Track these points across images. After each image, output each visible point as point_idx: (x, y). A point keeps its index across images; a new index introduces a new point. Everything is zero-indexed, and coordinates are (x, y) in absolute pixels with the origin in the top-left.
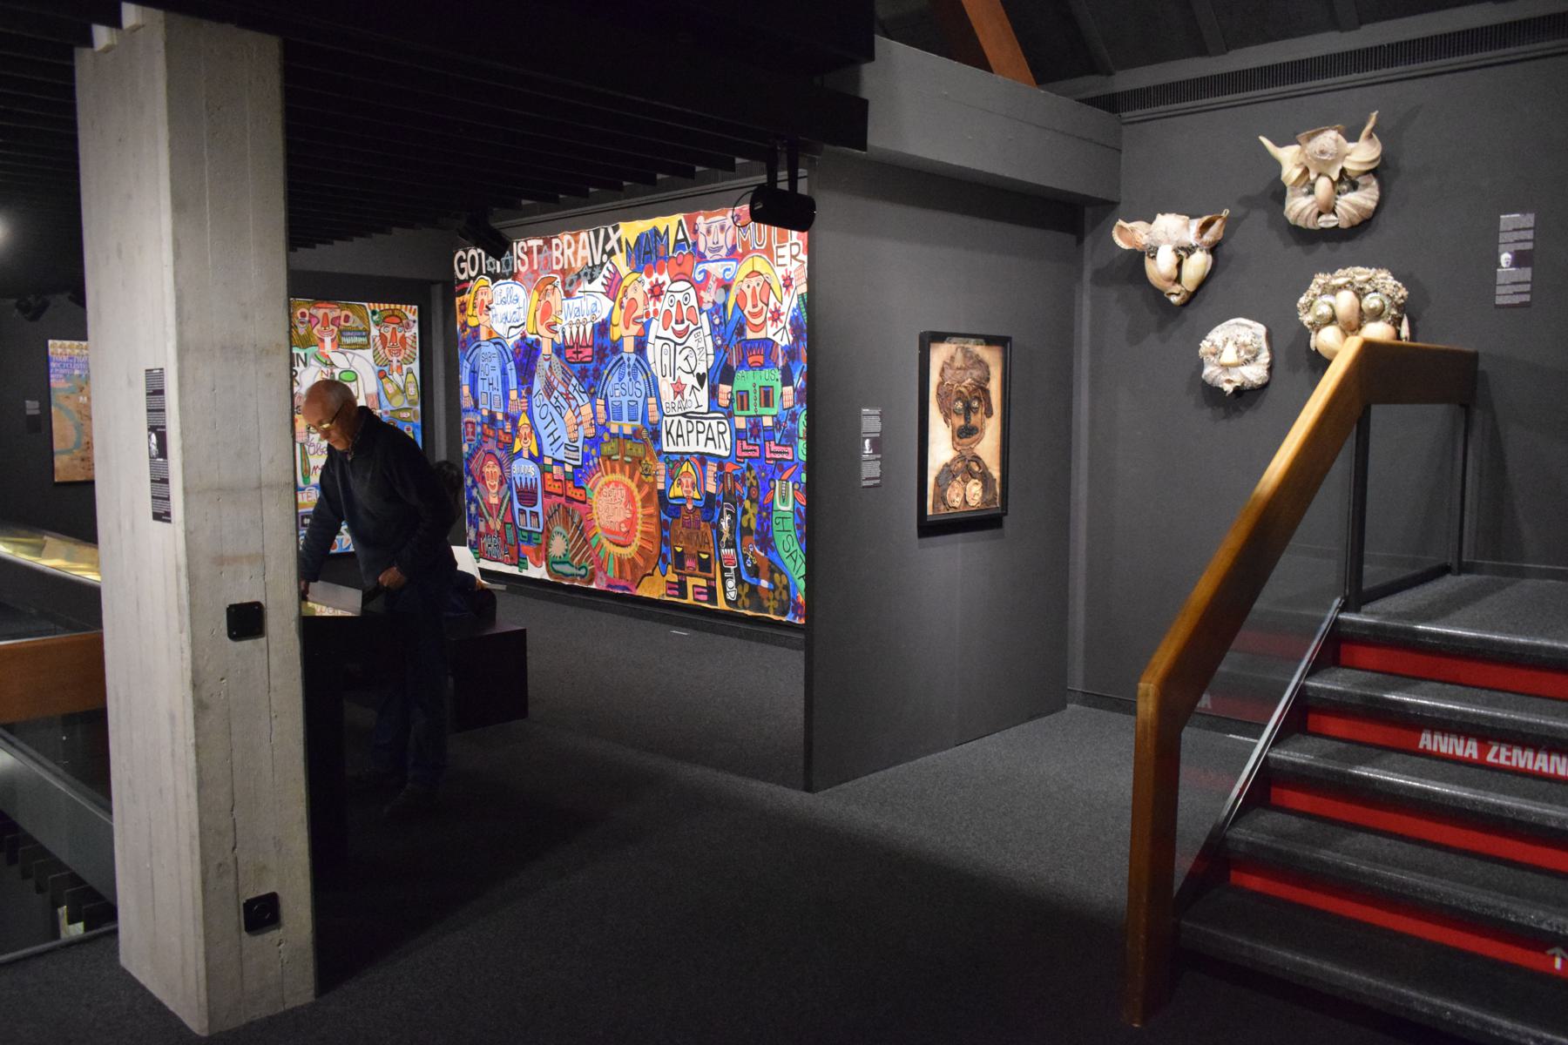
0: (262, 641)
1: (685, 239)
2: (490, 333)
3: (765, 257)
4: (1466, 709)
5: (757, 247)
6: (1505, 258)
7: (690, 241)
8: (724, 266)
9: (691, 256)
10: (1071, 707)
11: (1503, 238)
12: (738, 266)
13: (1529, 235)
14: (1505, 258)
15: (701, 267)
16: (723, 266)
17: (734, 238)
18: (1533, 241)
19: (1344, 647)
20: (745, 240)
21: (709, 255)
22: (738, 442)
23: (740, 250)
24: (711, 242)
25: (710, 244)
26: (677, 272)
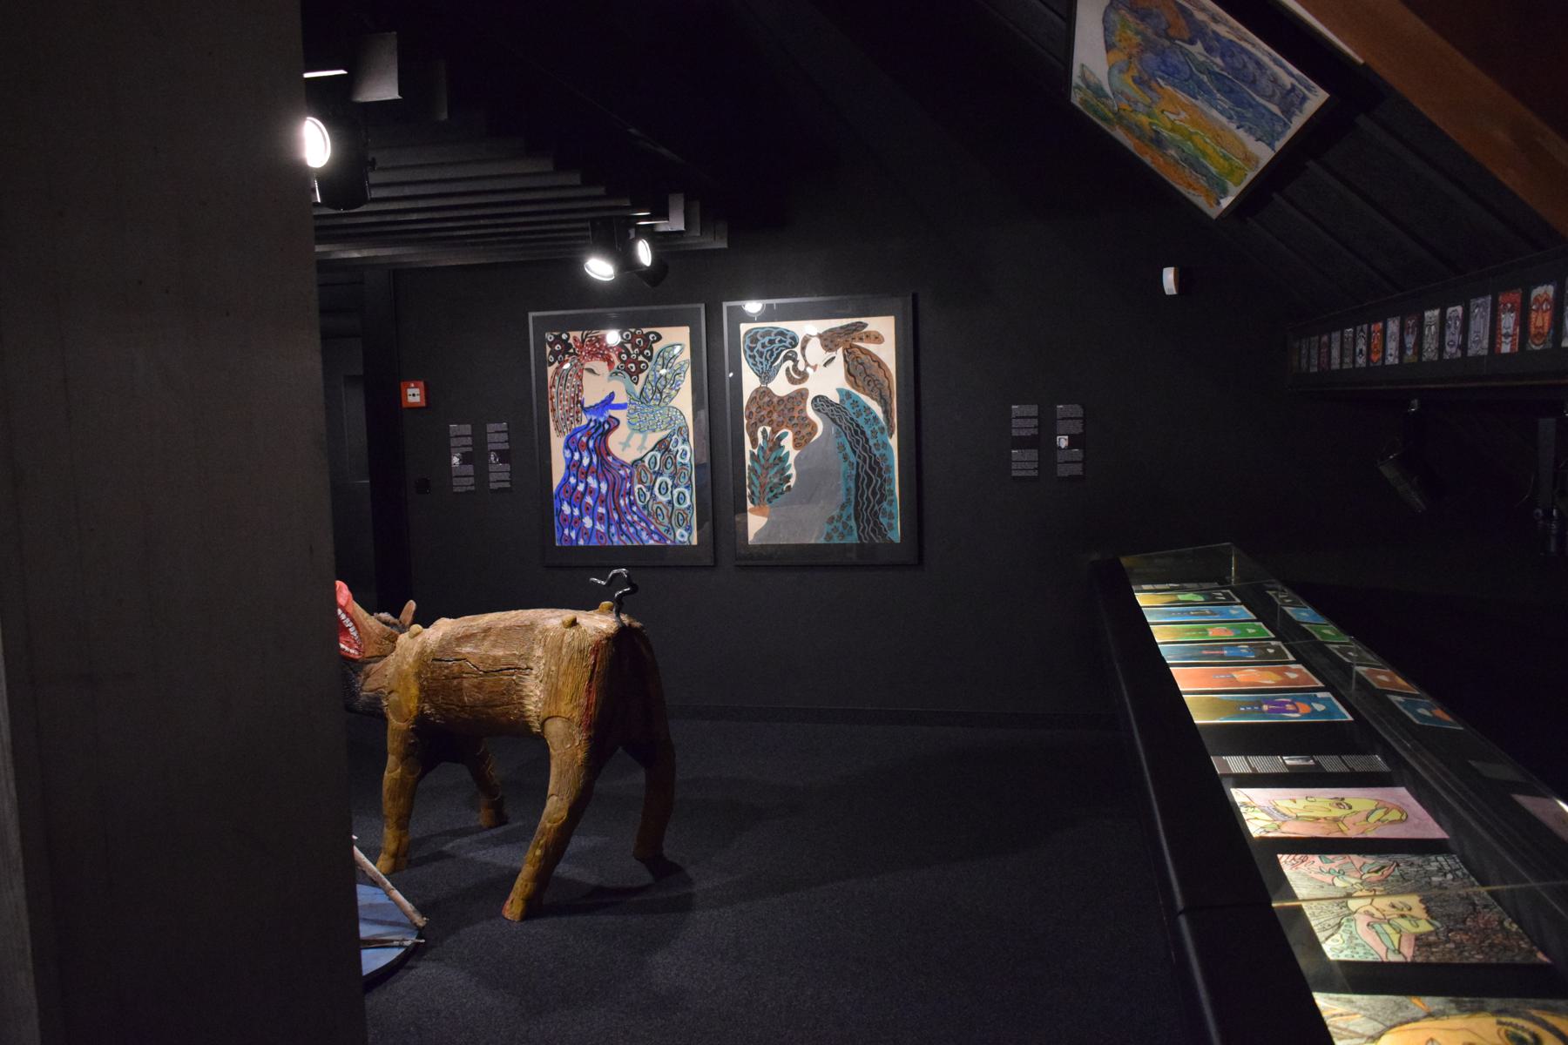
6: (455, 460)
11: (454, 442)
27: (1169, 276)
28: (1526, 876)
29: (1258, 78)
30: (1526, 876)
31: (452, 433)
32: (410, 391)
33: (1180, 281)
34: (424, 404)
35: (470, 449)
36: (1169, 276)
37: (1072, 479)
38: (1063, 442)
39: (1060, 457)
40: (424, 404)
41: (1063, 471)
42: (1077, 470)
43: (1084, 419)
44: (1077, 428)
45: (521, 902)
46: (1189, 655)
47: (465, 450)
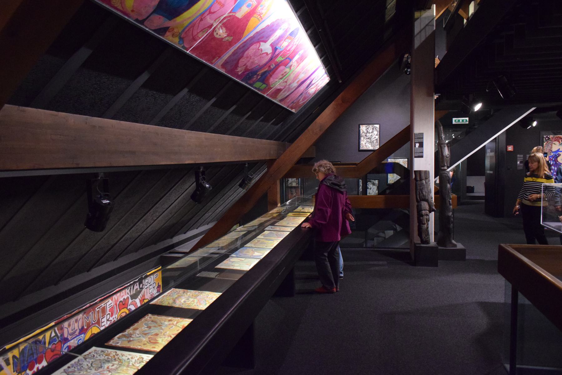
0: (373, 241)
1: (56, 335)
2: (157, 335)
3: (97, 325)
4: (137, 24)
5: (93, 322)
6: (518, 163)
7: (59, 335)
8: (77, 339)
9: (60, 343)
10: (417, 203)
11: (518, 159)
12: (85, 335)
13: (522, 158)
14: (518, 163)
15: (66, 345)
16: (77, 339)
17: (83, 322)
18: (523, 157)
19: (361, 148)
20: (88, 322)
21: (70, 337)
22: (298, 286)
23: (85, 327)
24: (71, 330)
25: (70, 331)
26: (52, 356)
32: (511, 148)
40: (513, 150)
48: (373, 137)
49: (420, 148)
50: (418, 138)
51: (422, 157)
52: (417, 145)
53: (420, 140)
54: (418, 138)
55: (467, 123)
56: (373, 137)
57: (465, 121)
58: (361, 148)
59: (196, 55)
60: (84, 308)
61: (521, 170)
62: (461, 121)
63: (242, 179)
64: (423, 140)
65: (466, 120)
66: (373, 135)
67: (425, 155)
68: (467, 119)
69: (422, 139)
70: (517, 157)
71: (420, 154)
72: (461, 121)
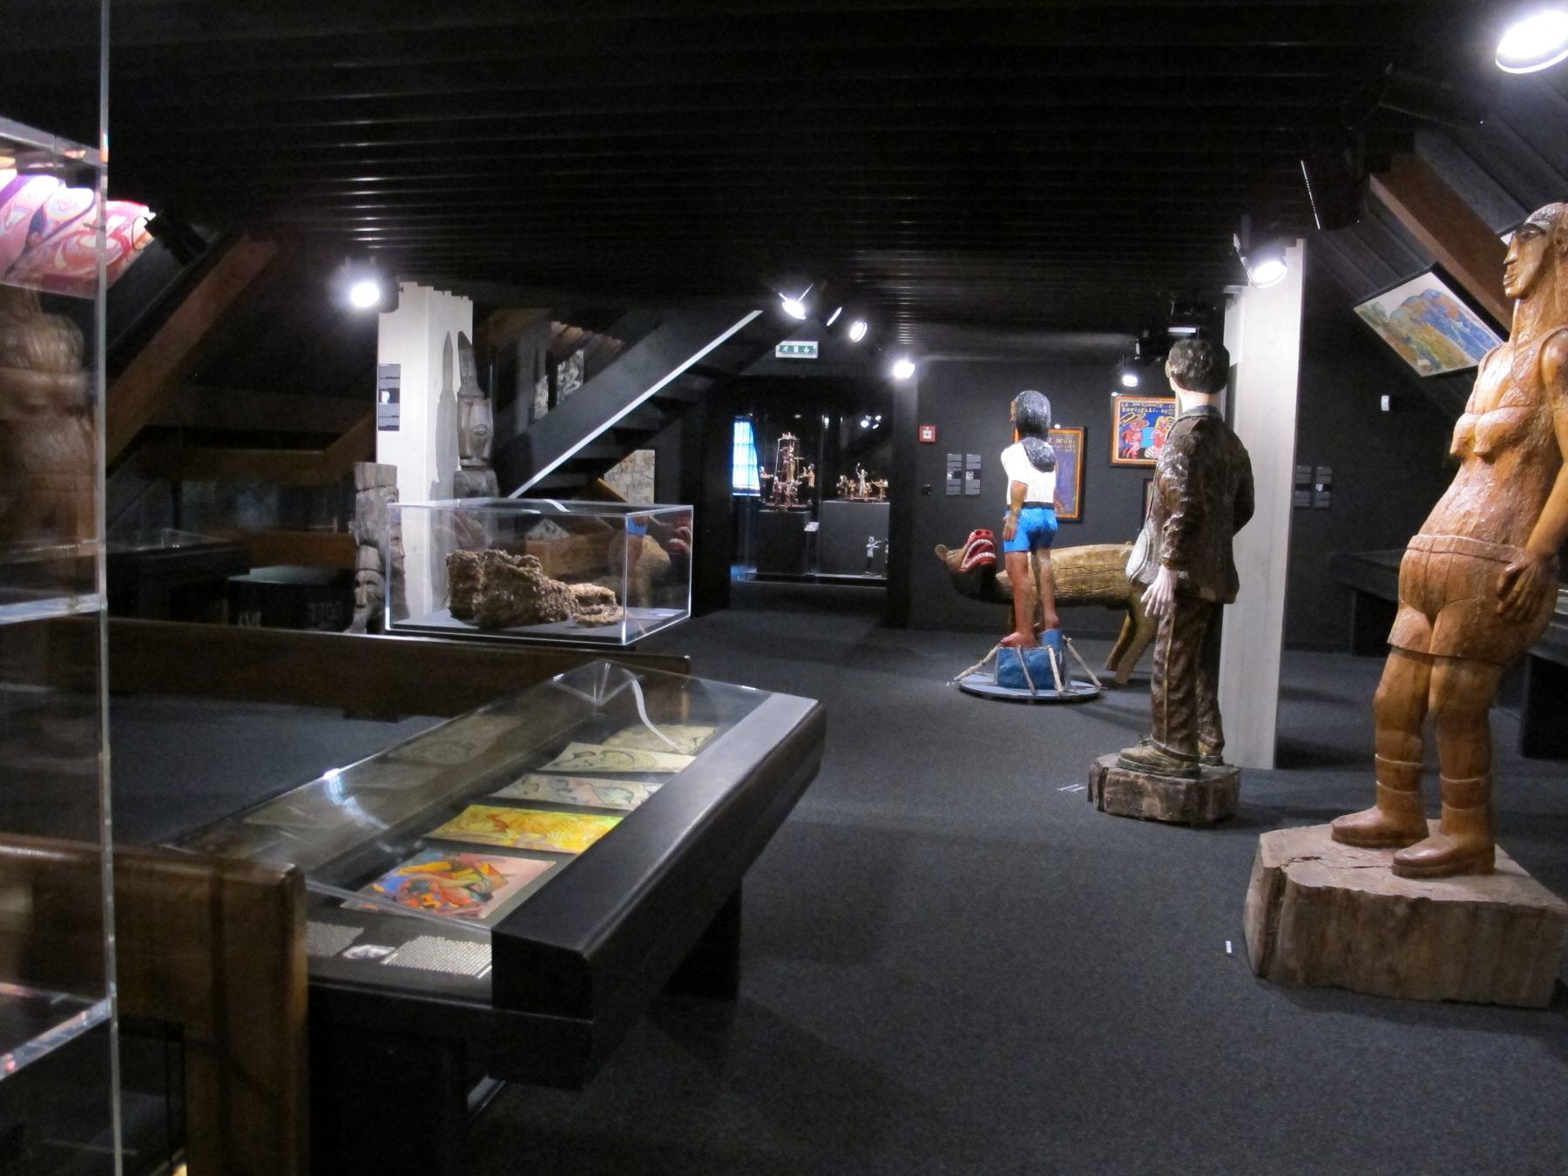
6: (950, 476)
11: (949, 465)
19: (1075, 516)
27: (1385, 402)
28: (1079, 658)
29: (1034, 442)
30: (1079, 658)
31: (949, 459)
32: (925, 432)
33: (1392, 403)
34: (934, 440)
35: (960, 469)
36: (1385, 402)
37: (1323, 509)
38: (1320, 487)
39: (1318, 496)
40: (934, 440)
41: (1319, 504)
42: (1325, 504)
43: (1332, 476)
44: (1328, 480)
45: (647, 577)
46: (564, 570)
47: (956, 470)
48: (568, 385)
49: (392, 405)
50: (387, 378)
51: (396, 428)
52: (386, 396)
53: (392, 384)
54: (387, 378)
55: (815, 356)
56: (568, 385)
57: (806, 350)
58: (1075, 516)
59: (126, 1160)
60: (418, 191)
61: (956, 496)
62: (796, 349)
63: (337, 180)
64: (399, 384)
65: (811, 348)
66: (568, 378)
67: (402, 423)
68: (815, 345)
69: (397, 380)
70: (946, 461)
71: (392, 422)
72: (796, 349)
